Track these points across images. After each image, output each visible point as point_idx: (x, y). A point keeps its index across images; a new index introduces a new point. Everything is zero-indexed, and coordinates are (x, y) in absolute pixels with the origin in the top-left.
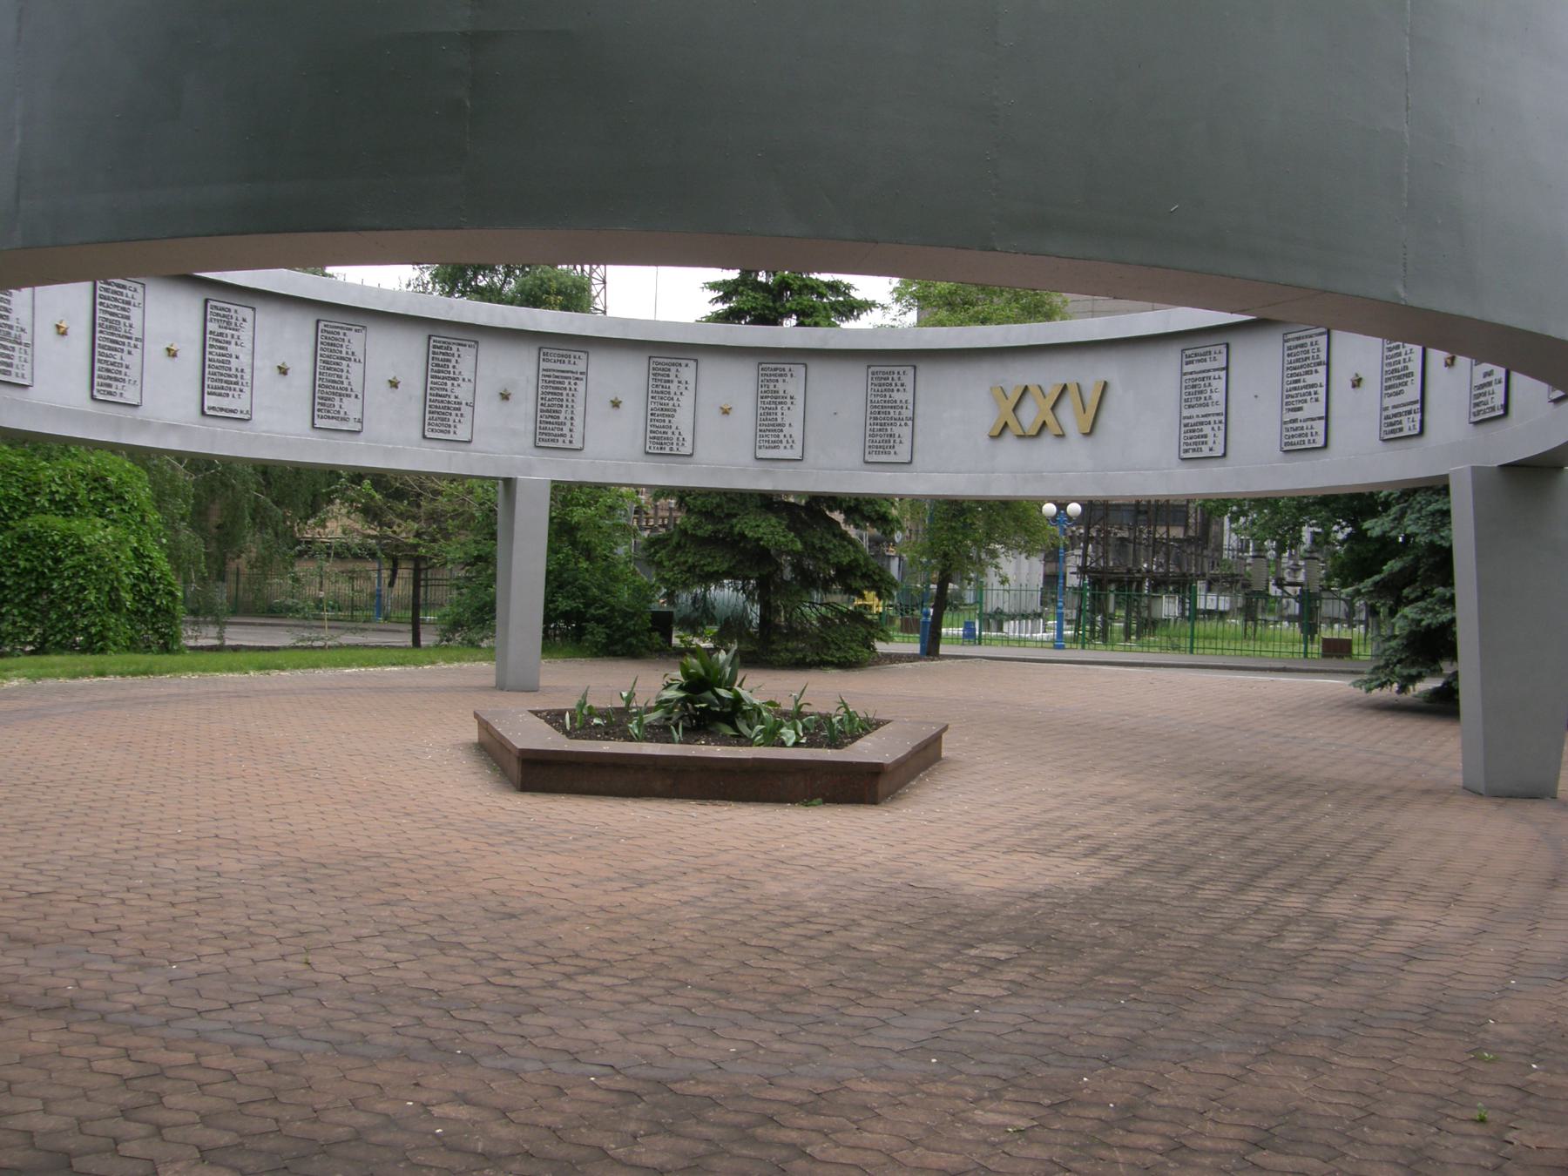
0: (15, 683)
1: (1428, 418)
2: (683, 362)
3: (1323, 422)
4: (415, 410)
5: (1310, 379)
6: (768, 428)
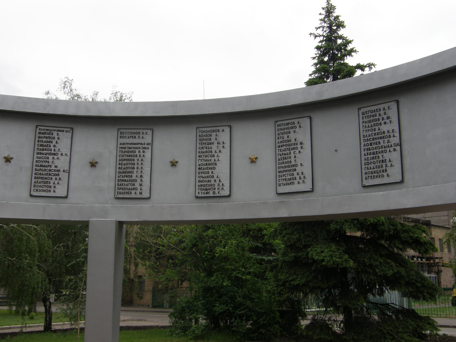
2: (221, 129)
4: (25, 177)
6: (286, 169)
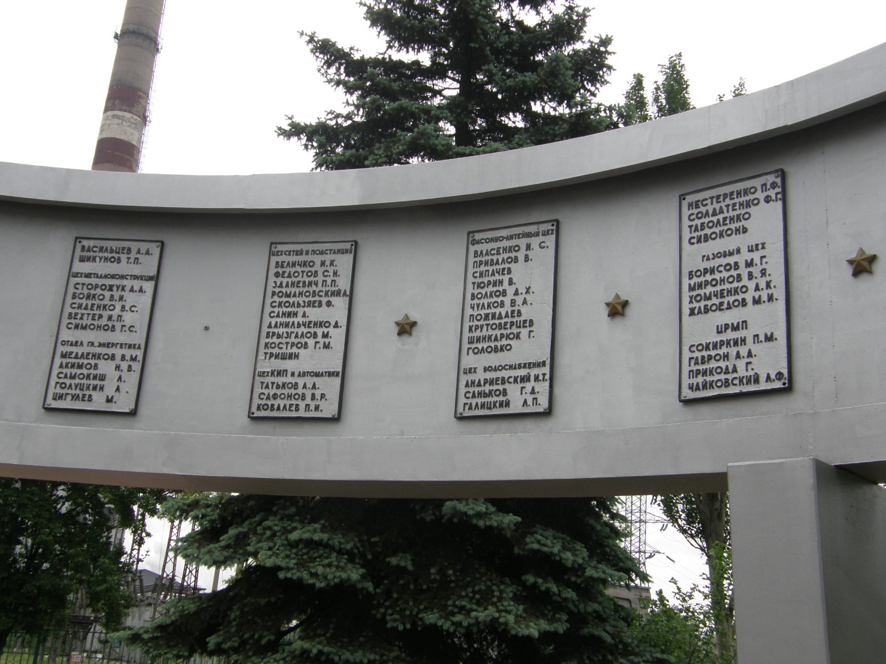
0: (358, 656)
1: (557, 390)
3: (338, 380)
5: (315, 314)
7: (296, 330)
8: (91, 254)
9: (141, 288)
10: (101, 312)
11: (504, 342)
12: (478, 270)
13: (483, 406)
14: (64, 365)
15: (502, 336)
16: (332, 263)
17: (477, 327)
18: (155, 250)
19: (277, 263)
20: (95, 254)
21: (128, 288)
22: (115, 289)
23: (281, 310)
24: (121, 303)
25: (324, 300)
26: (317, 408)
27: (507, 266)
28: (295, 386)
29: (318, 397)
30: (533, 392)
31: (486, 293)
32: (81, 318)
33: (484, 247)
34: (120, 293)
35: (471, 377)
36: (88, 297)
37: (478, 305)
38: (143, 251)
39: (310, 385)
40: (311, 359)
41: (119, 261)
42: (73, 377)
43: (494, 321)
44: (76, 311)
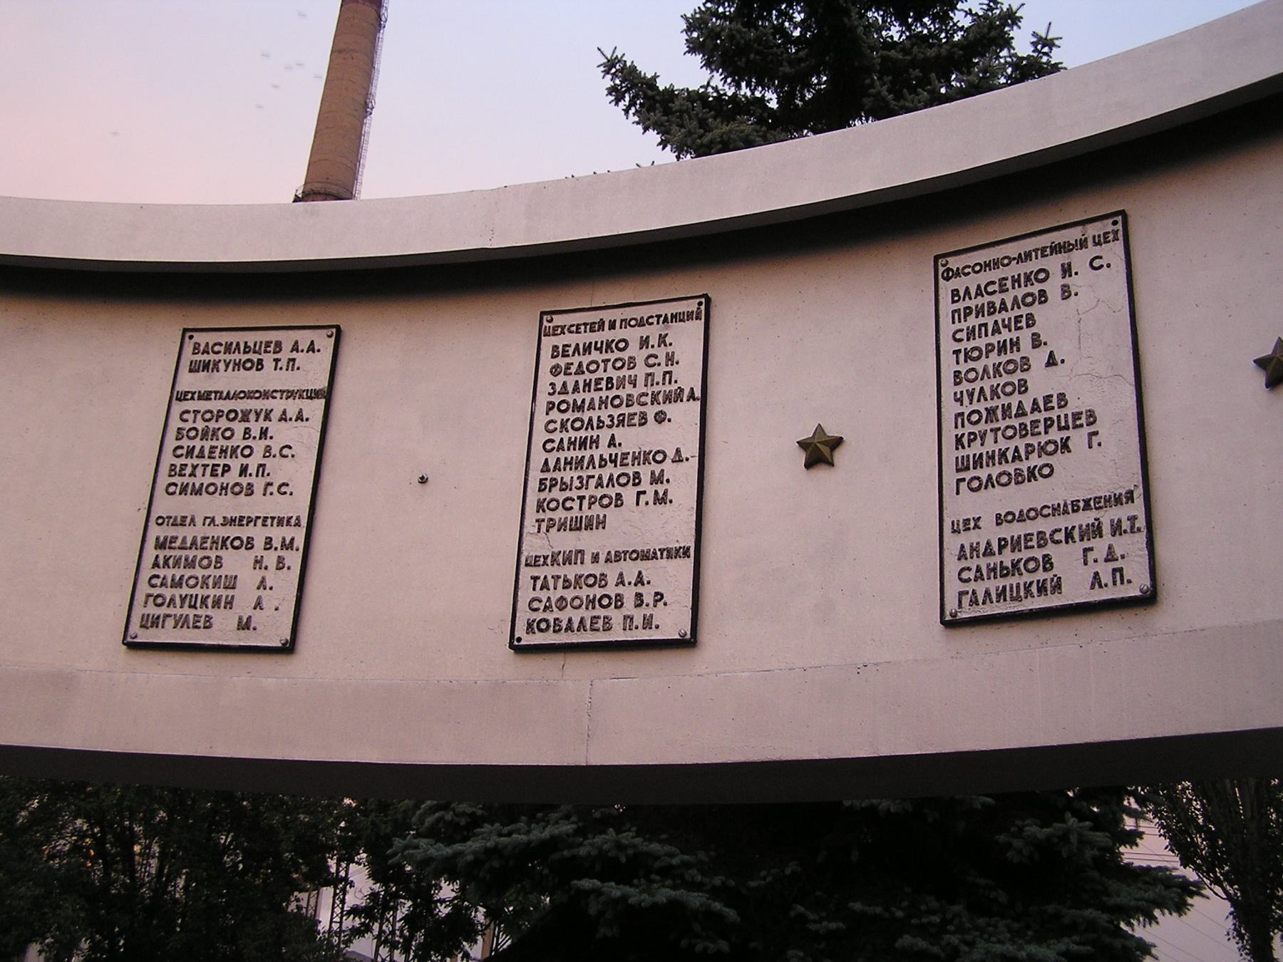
5: (631, 439)
7: (596, 473)
8: (212, 357)
9: (300, 411)
10: (228, 461)
11: (1035, 461)
12: (963, 325)
13: (1002, 594)
14: (161, 562)
15: (1030, 449)
16: (662, 340)
17: (972, 437)
18: (325, 343)
19: (555, 348)
20: (217, 357)
21: (276, 415)
22: (252, 417)
23: (565, 436)
24: (264, 443)
25: (651, 411)
26: (648, 623)
27: (1024, 311)
28: (601, 580)
29: (649, 599)
30: (1110, 557)
31: (985, 370)
32: (193, 474)
33: (972, 282)
34: (263, 424)
35: (967, 538)
36: (205, 436)
37: (971, 395)
38: (304, 345)
39: (631, 577)
40: (636, 524)
41: (260, 365)
42: (177, 584)
43: (1008, 422)
44: (183, 461)
